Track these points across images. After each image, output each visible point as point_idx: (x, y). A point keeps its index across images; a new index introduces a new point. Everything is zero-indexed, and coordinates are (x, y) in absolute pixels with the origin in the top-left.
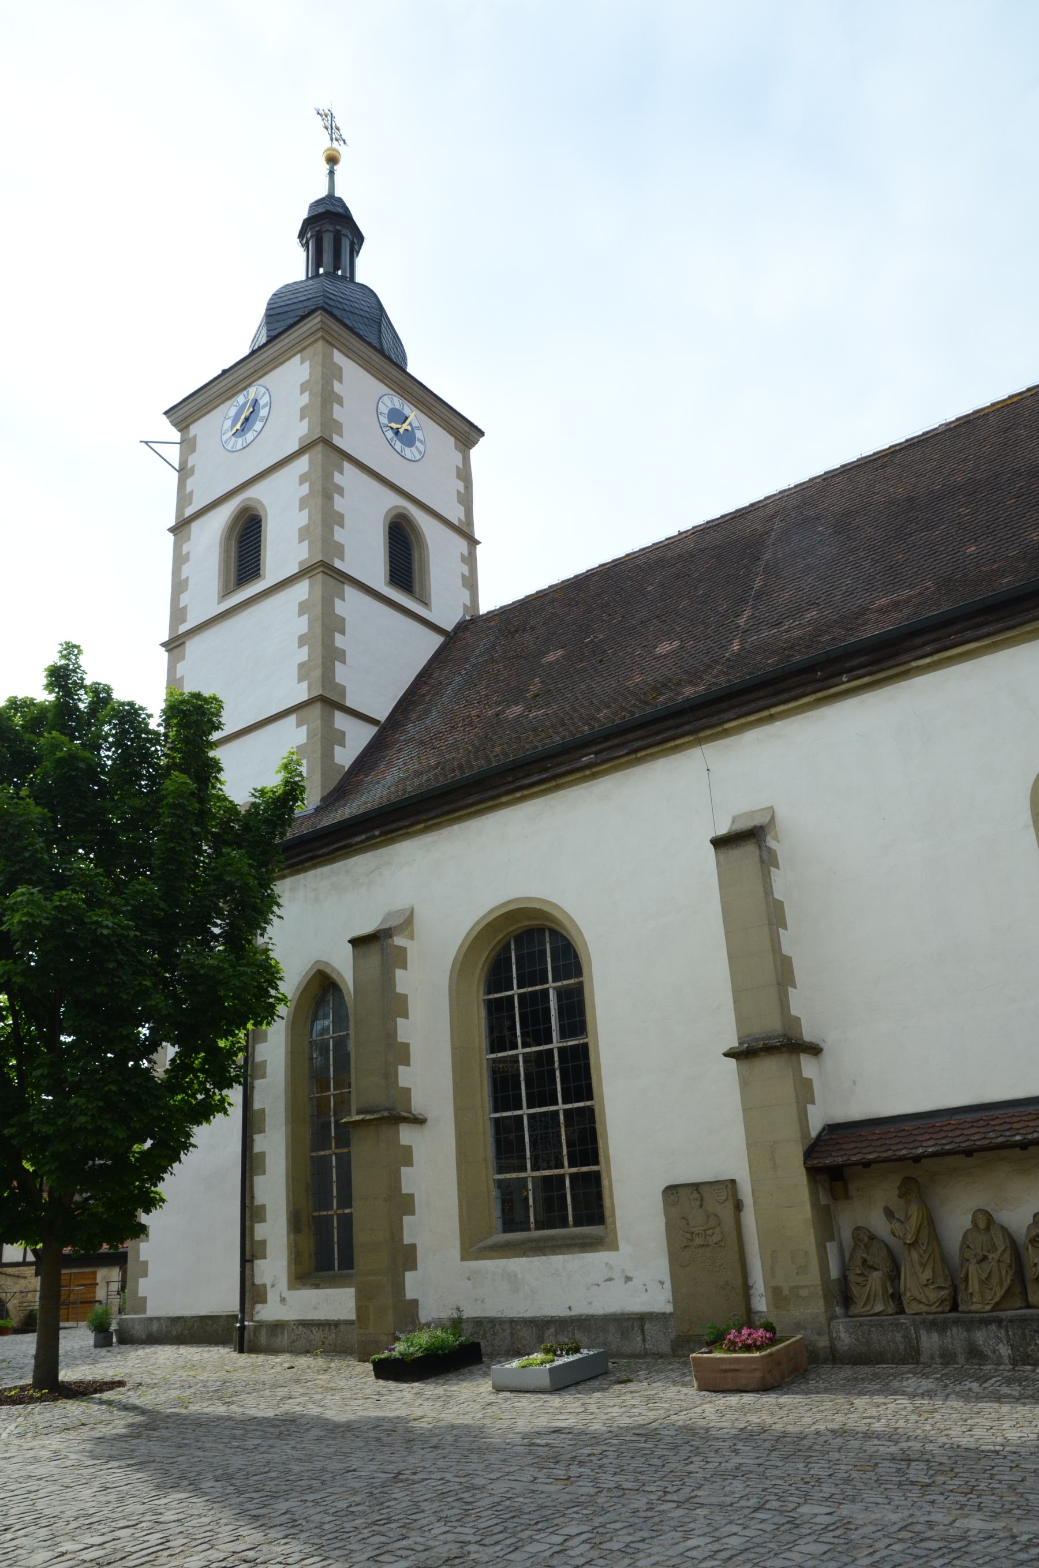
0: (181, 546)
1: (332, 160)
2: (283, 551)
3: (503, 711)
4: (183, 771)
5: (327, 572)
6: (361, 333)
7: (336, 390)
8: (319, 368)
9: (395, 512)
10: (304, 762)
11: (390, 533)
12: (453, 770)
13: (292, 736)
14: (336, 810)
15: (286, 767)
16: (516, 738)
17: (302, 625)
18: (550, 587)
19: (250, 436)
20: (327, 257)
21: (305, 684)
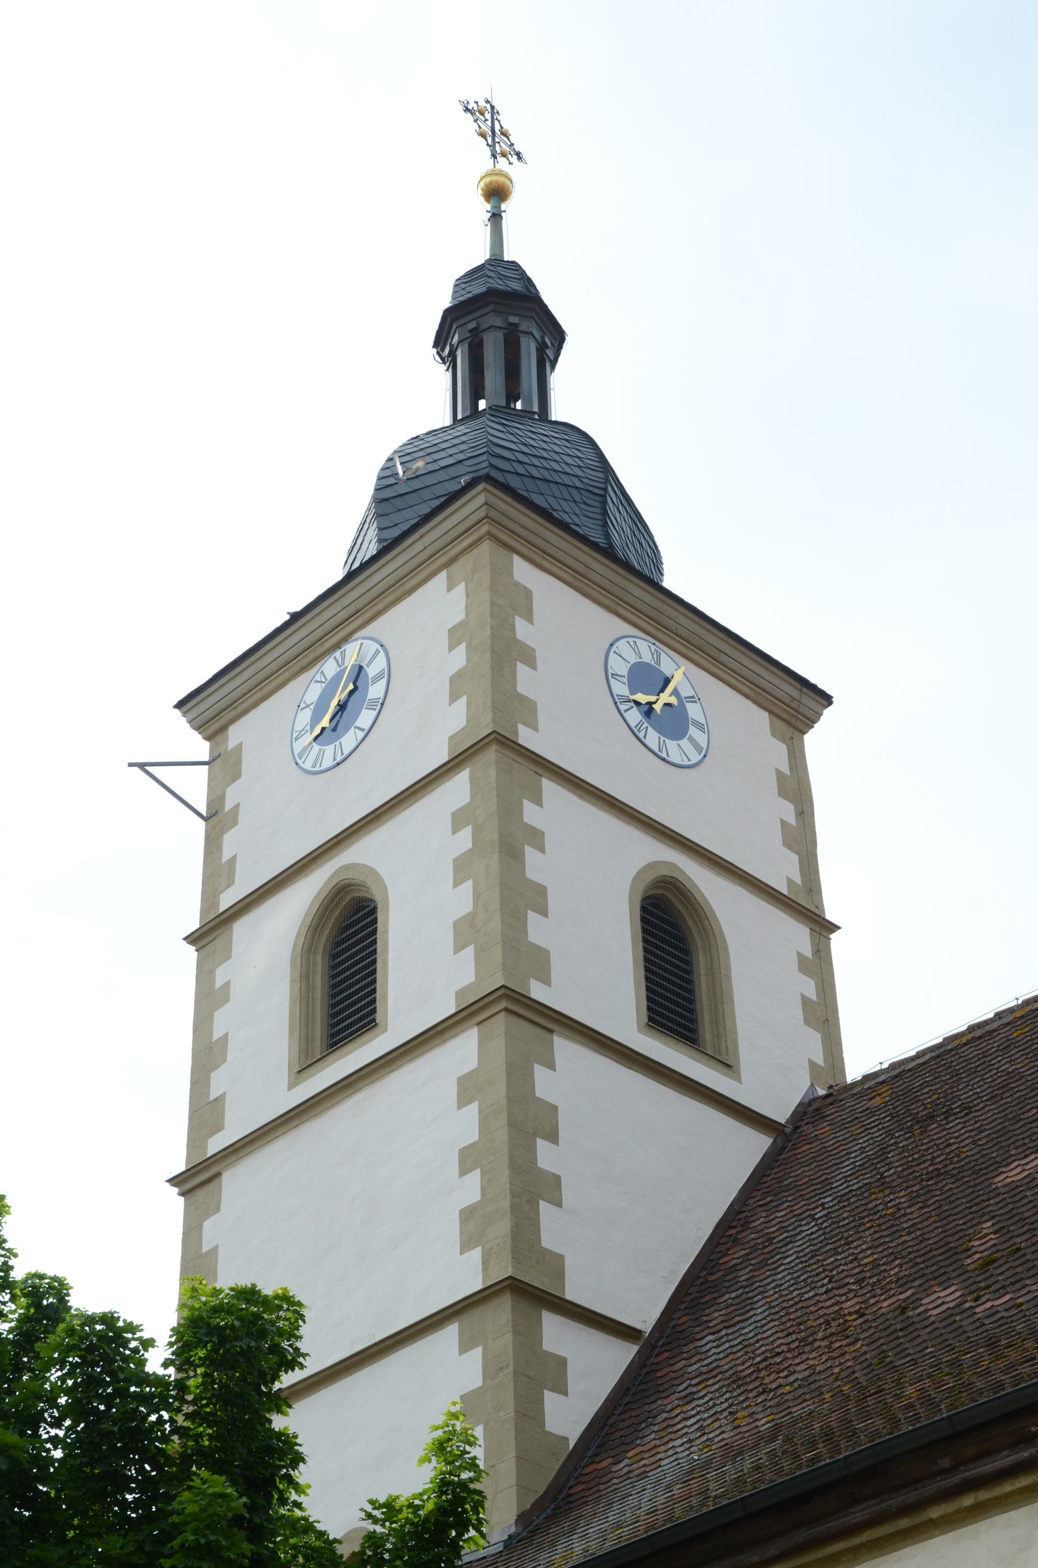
0: (212, 972)
1: (497, 193)
2: (422, 971)
3: (915, 1301)
4: (217, 1468)
5: (515, 1010)
6: (566, 518)
7: (520, 635)
8: (486, 596)
9: (651, 876)
10: (479, 1432)
11: (643, 920)
12: (812, 1444)
13: (449, 1374)
14: (553, 1544)
15: (441, 1447)
16: (951, 1364)
17: (465, 1125)
18: (999, 1015)
19: (349, 740)
20: (494, 377)
21: (476, 1255)
